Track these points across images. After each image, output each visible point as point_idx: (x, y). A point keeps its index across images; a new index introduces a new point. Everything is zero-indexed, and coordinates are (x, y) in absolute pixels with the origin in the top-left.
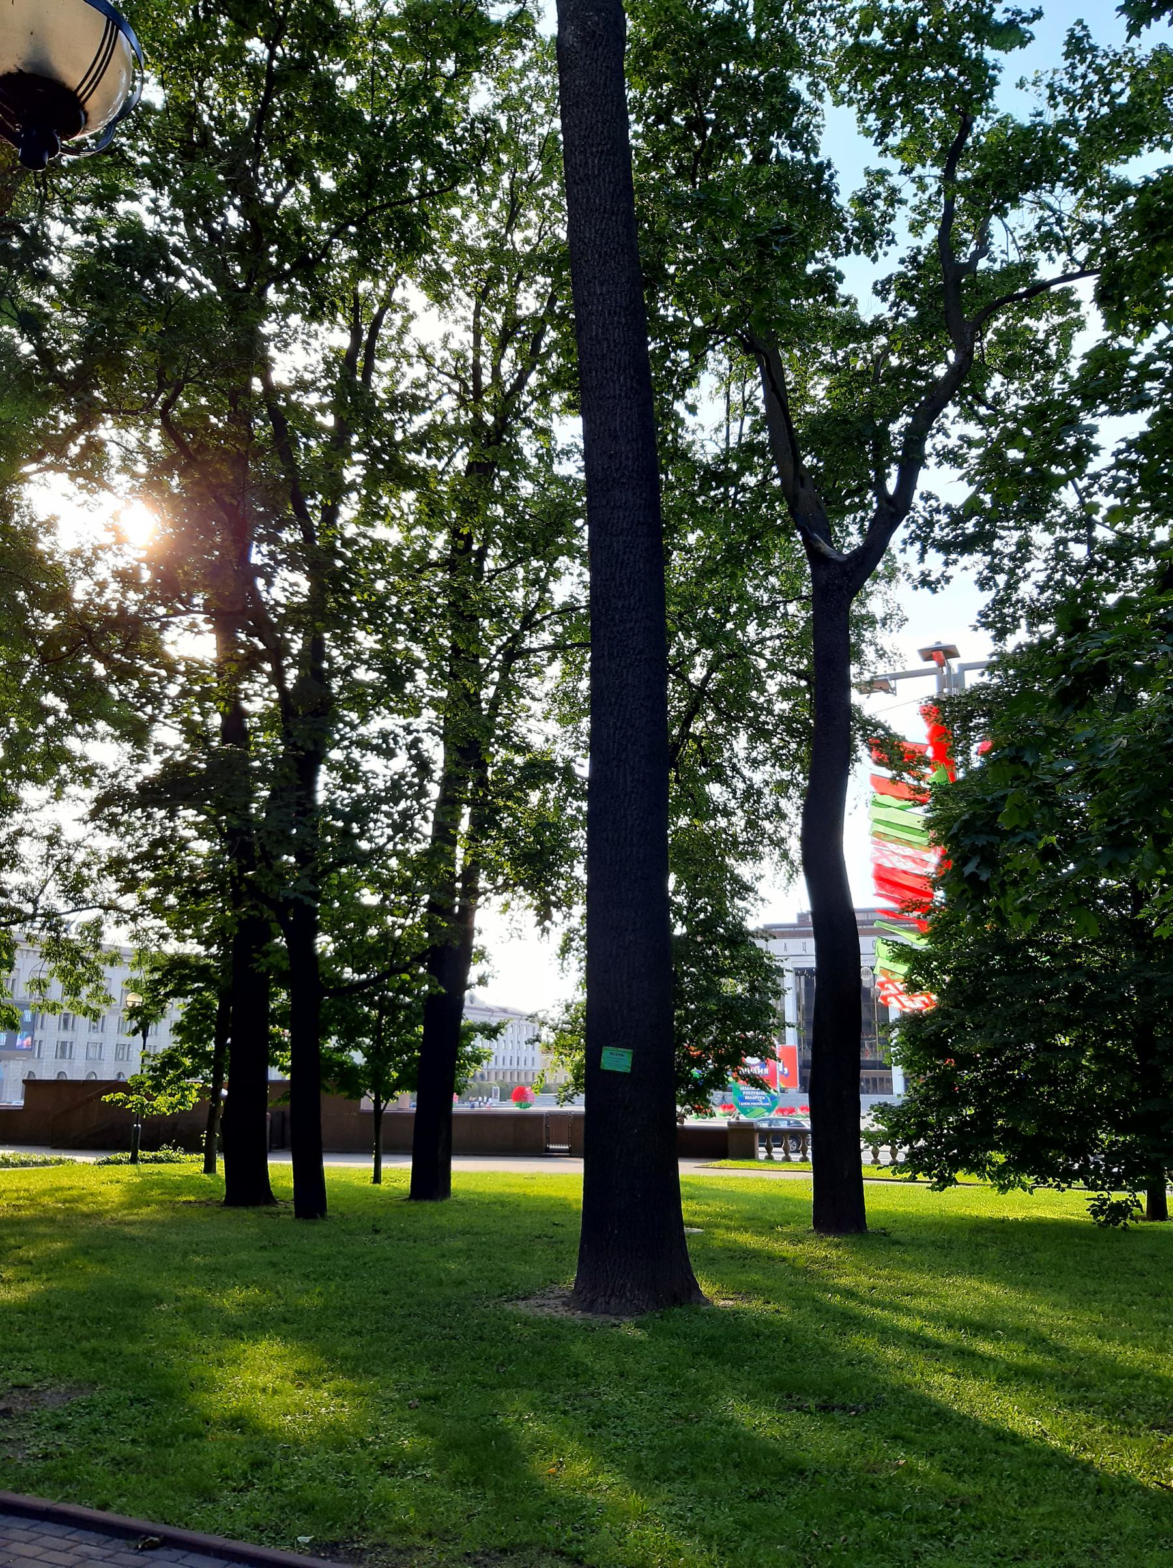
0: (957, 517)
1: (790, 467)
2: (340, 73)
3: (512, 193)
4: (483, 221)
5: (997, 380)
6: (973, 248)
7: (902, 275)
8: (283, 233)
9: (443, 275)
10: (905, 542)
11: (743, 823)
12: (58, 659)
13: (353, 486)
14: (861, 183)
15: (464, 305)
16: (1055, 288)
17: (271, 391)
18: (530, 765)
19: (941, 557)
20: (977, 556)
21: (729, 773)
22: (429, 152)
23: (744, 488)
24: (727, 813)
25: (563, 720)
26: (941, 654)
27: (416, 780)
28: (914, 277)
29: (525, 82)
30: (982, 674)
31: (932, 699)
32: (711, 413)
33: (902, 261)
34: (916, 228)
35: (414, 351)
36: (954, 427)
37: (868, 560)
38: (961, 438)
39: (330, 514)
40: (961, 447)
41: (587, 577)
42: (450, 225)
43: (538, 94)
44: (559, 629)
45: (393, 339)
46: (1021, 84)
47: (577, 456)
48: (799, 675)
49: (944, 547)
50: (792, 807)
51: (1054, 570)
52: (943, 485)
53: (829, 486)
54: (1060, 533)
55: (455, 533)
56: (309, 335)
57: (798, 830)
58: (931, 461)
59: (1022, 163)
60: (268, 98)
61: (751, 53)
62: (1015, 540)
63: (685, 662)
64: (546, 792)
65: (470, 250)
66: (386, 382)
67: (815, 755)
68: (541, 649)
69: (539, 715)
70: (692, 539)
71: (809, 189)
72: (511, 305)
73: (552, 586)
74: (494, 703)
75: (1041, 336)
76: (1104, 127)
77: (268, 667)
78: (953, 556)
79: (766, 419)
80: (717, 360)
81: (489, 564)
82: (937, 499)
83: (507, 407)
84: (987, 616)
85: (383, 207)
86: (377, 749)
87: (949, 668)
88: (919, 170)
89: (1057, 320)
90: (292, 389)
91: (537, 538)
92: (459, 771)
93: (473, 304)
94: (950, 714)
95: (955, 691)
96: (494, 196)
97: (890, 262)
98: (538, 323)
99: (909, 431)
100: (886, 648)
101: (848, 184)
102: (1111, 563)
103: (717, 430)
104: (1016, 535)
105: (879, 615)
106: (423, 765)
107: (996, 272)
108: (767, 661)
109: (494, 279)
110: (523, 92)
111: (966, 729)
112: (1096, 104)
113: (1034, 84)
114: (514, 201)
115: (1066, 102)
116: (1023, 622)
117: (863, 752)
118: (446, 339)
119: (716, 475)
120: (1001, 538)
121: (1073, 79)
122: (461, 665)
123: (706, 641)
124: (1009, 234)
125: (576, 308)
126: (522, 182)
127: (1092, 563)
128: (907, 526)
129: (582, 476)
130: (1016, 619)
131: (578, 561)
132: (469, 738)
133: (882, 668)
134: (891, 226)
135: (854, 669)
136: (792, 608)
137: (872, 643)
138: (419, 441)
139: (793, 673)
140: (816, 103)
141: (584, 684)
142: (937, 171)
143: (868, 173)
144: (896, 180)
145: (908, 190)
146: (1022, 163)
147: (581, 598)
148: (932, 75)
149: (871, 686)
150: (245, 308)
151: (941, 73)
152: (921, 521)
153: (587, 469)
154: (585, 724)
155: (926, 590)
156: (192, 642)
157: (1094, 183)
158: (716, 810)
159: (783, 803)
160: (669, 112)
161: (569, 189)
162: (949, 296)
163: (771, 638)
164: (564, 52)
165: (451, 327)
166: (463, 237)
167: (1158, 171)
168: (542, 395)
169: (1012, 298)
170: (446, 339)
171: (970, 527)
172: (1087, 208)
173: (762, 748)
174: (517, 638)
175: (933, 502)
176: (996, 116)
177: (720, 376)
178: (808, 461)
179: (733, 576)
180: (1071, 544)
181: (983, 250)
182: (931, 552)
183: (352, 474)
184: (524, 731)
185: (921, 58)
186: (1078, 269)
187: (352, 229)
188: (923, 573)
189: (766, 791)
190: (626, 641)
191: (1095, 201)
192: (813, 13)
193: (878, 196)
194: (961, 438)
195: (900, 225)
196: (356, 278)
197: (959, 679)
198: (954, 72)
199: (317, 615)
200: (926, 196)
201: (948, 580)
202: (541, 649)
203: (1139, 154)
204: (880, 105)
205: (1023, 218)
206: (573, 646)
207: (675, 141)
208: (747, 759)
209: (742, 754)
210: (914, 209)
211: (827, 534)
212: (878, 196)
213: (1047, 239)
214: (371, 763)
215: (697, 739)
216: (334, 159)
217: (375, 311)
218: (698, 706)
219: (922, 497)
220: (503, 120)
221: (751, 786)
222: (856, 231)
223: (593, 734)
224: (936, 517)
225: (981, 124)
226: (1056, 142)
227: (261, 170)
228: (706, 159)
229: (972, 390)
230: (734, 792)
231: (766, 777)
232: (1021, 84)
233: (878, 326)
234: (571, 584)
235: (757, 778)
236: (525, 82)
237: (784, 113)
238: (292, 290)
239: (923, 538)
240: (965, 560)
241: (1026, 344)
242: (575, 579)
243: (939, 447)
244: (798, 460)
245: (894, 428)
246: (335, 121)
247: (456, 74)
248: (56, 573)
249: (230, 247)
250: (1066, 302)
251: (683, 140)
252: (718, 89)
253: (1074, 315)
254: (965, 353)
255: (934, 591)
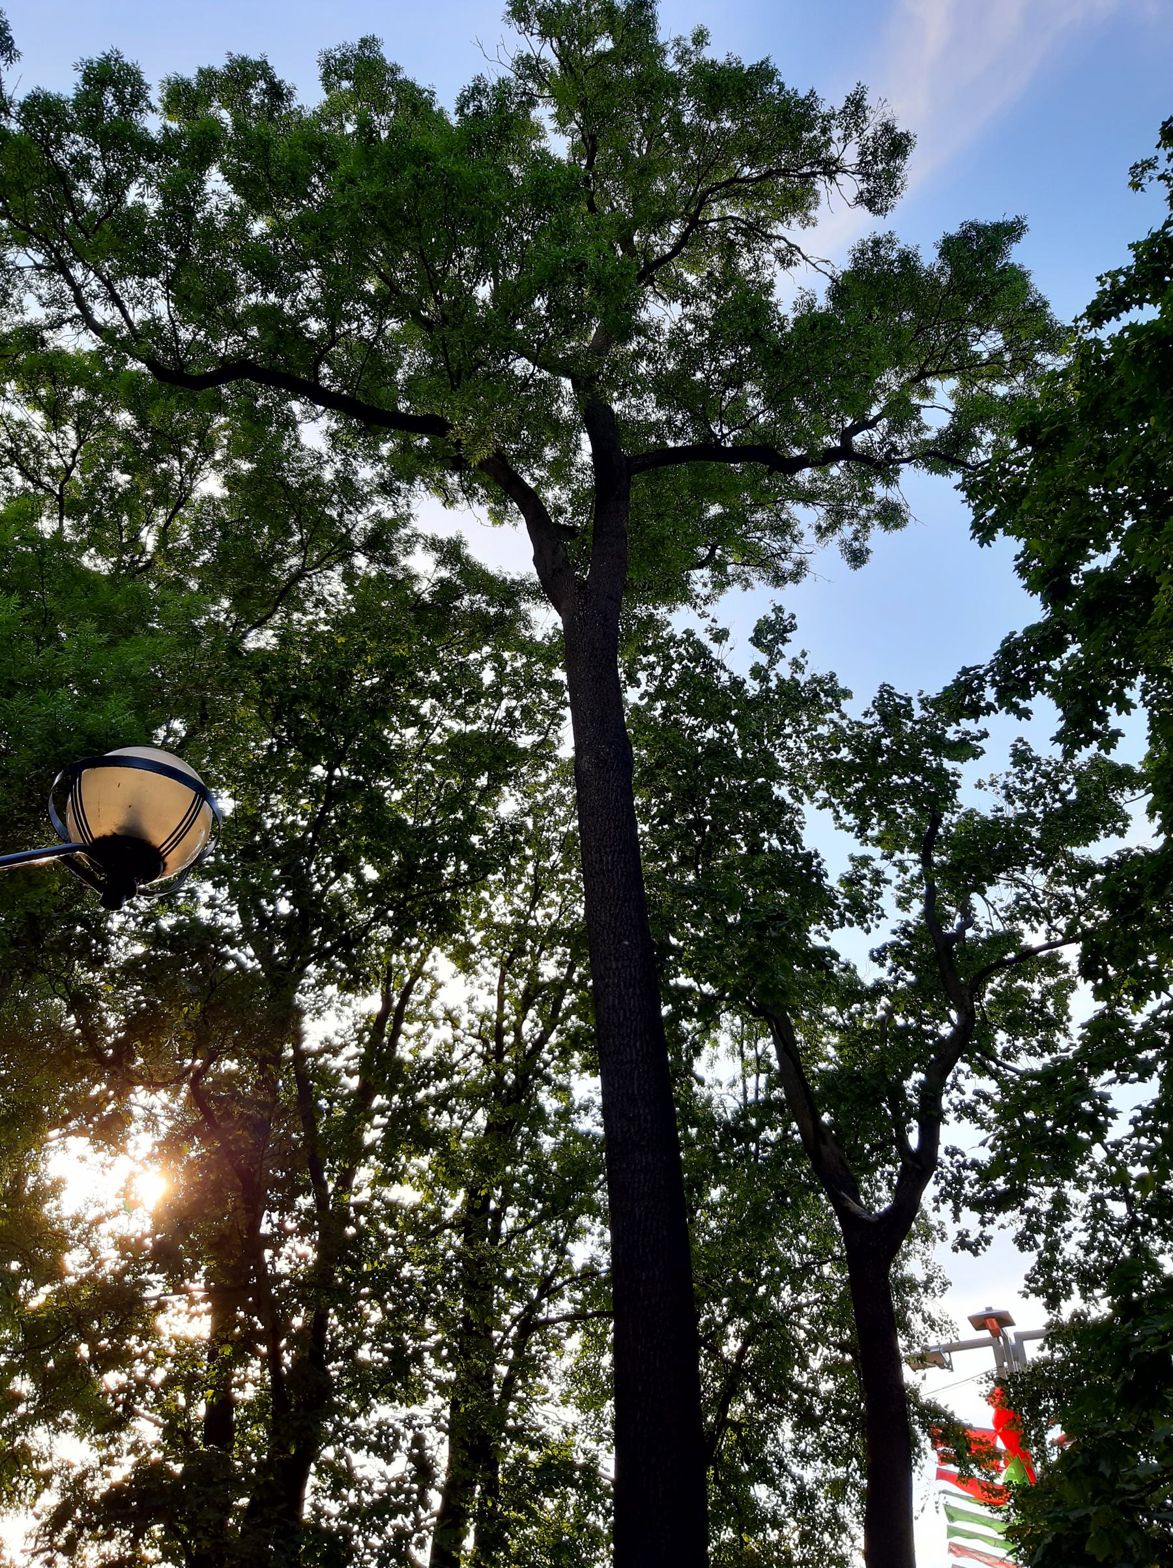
0: (986, 1174)
1: (809, 1124)
2: (388, 788)
3: (535, 877)
5: (1001, 1038)
6: (958, 920)
8: (327, 917)
9: (471, 948)
10: (936, 1200)
11: (796, 1535)
12: (39, 1337)
13: (371, 1149)
14: (848, 867)
15: (489, 972)
16: (1043, 953)
18: (547, 1465)
19: (976, 1216)
22: (463, 851)
23: (766, 1143)
24: (777, 1524)
25: (585, 1404)
27: (415, 1486)
28: (908, 946)
29: (549, 792)
30: (1042, 1349)
31: (989, 1377)
32: (724, 1071)
33: (894, 932)
34: (903, 904)
35: (440, 1014)
36: (968, 1083)
37: (903, 1218)
38: (976, 1093)
39: (345, 1181)
40: (978, 1102)
41: (608, 1237)
44: (579, 1295)
45: (421, 1004)
46: (979, 785)
47: (595, 1110)
48: (843, 1347)
49: (977, 1205)
50: (850, 1512)
51: (1095, 1230)
52: (964, 1140)
53: (850, 1136)
55: (472, 1193)
56: (343, 1004)
57: (861, 1543)
58: (950, 1117)
60: (324, 810)
61: (744, 769)
63: (717, 1335)
64: (565, 1497)
65: (498, 926)
67: (871, 1448)
68: (559, 1320)
69: (557, 1399)
70: (715, 1194)
71: (802, 874)
72: (534, 974)
74: (509, 1382)
75: (1036, 996)
76: (1060, 818)
77: (264, 1349)
79: (780, 1074)
80: (730, 1021)
81: (507, 1224)
82: (963, 1155)
83: (529, 1067)
84: (1036, 1281)
85: (420, 895)
87: (1005, 1338)
88: (898, 856)
89: (1050, 981)
90: (320, 1053)
91: (560, 1201)
92: (466, 1473)
93: (498, 972)
94: (1017, 1393)
95: (1017, 1367)
96: (520, 882)
97: (883, 934)
100: (935, 1316)
102: (1154, 1221)
103: (733, 1084)
104: (1050, 1191)
105: (920, 1277)
106: (423, 1469)
107: (983, 941)
108: (806, 1331)
109: (520, 951)
110: (547, 800)
111: (1036, 1414)
112: (1049, 800)
115: (1022, 800)
116: (1075, 1286)
118: (470, 1001)
119: (739, 1130)
120: (1035, 1195)
121: (1024, 782)
122: (471, 1342)
123: (738, 1310)
124: (990, 907)
126: (545, 869)
127: (1134, 1222)
129: (600, 1131)
130: (1067, 1284)
131: (598, 1220)
132: (479, 1432)
135: (902, 1342)
136: (826, 1270)
137: (917, 1310)
138: (441, 1102)
139: (838, 1346)
141: (607, 1360)
142: (916, 856)
143: (852, 859)
144: (878, 864)
145: (891, 872)
147: (603, 1261)
148: (900, 782)
149: (923, 1360)
150: (282, 980)
151: (908, 780)
154: (609, 1408)
156: (186, 1320)
157: (1062, 863)
158: (765, 1520)
159: (843, 1510)
160: (672, 816)
162: (942, 962)
165: (476, 992)
166: (491, 915)
167: (1118, 853)
168: (565, 1054)
170: (470, 1001)
171: (1000, 1183)
172: (1059, 883)
173: (809, 1442)
174: (533, 1307)
175: (958, 1157)
176: (962, 811)
177: (733, 1036)
178: (826, 1118)
179: (761, 1238)
180: (1108, 1201)
182: (965, 1211)
183: (372, 1136)
184: (540, 1421)
185: (888, 769)
187: (391, 913)
188: (960, 1234)
189: (820, 1493)
190: (651, 1310)
191: (1064, 878)
192: (790, 736)
194: (976, 1093)
195: (888, 899)
198: (918, 778)
200: (908, 877)
201: (988, 1241)
202: (559, 1320)
203: (1096, 839)
205: (1002, 893)
207: (678, 838)
208: (796, 1453)
209: (788, 1447)
210: (898, 888)
211: (855, 1191)
212: (864, 877)
213: (1025, 910)
214: (366, 1465)
215: (737, 1427)
216: (378, 857)
217: (407, 979)
218: (735, 1385)
219: (947, 1152)
220: (529, 822)
221: (801, 1488)
222: (847, 907)
223: (617, 1423)
224: (965, 1173)
225: (948, 818)
226: (1019, 832)
227: (313, 867)
228: (707, 850)
231: (819, 1475)
232: (979, 785)
233: (879, 989)
234: (590, 1247)
235: (810, 1474)
236: (549, 792)
237: (776, 816)
238: (331, 965)
239: (952, 1193)
240: (1002, 1218)
242: (596, 1239)
243: (956, 1102)
244: (817, 1117)
245: (909, 1084)
246: (381, 829)
247: (488, 787)
248: (60, 1242)
249: (278, 931)
250: (1053, 965)
252: (712, 797)
253: (1065, 976)
254: (967, 1014)
255: (976, 1254)
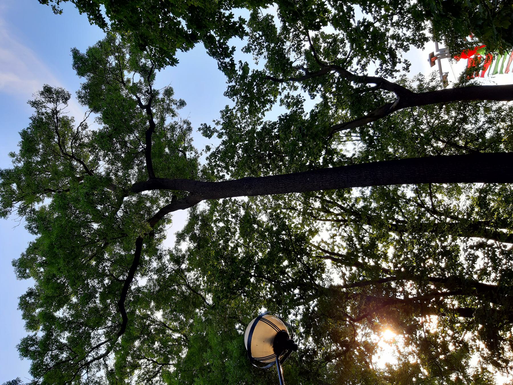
0: (384, 61)
1: (368, 119)
2: (258, 257)
3: (287, 209)
4: (295, 218)
5: (339, 56)
6: (301, 70)
7: (309, 91)
8: (300, 277)
9: (310, 230)
10: (393, 78)
12: (437, 371)
13: (376, 263)
14: (284, 106)
15: (318, 224)
17: (345, 286)
18: (479, 205)
19: (398, 64)
20: (397, 53)
21: (481, 130)
22: (278, 232)
23: (374, 133)
24: (499, 130)
25: (459, 193)
26: (432, 59)
27: (486, 248)
29: (259, 204)
30: (441, 43)
32: (350, 147)
33: (305, 91)
34: (296, 88)
35: (332, 240)
36: (354, 67)
37: (399, 89)
38: (358, 64)
39: (386, 271)
40: (361, 64)
41: (405, 185)
42: (296, 227)
43: (262, 201)
44: (424, 195)
46: (257, 63)
47: (363, 189)
48: (441, 108)
49: (394, 64)
50: (495, 106)
51: (402, 26)
52: (373, 68)
53: (372, 106)
54: (389, 26)
55: (390, 230)
56: (328, 272)
57: (505, 102)
58: (365, 73)
59: (279, 61)
60: (265, 278)
61: (251, 141)
62: (391, 41)
63: (437, 150)
64: (490, 199)
65: (303, 221)
66: (341, 249)
67: (474, 99)
68: (432, 201)
69: (458, 202)
70: (391, 150)
71: (286, 122)
72: (319, 209)
73: (408, 198)
78: (397, 60)
79: (352, 129)
80: (334, 145)
81: (401, 218)
85: (293, 247)
86: (474, 261)
87: (438, 55)
88: (280, 90)
90: (345, 279)
91: (393, 201)
92: (482, 232)
93: (318, 221)
94: (456, 51)
95: (447, 51)
96: (288, 214)
97: (305, 95)
98: (323, 201)
99: (356, 82)
100: (430, 78)
101: (284, 111)
102: (399, 6)
103: (355, 144)
104: (390, 41)
105: (418, 83)
106: (481, 246)
107: (308, 62)
110: (262, 205)
111: (463, 45)
112: (262, 41)
113: (257, 60)
114: (289, 208)
115: (262, 49)
116: (421, 32)
117: (472, 81)
118: (327, 230)
119: (370, 142)
121: (256, 49)
122: (439, 230)
124: (297, 60)
125: (319, 190)
127: (400, 13)
128: (387, 77)
129: (370, 188)
130: (420, 35)
131: (399, 188)
132: (469, 228)
133: (438, 78)
134: (295, 96)
135: (439, 89)
137: (429, 84)
138: (361, 240)
140: (263, 123)
141: (445, 186)
142: (280, 84)
143: (281, 105)
144: (283, 96)
145: (285, 93)
146: (279, 61)
149: (445, 81)
150: (320, 292)
151: (255, 87)
152: (385, 73)
153: (368, 185)
154: (461, 185)
155: (410, 68)
156: (432, 323)
158: (497, 134)
159: (494, 108)
160: (267, 164)
161: (286, 192)
162: (315, 75)
163: (427, 120)
164: (252, 195)
165: (324, 228)
167: (279, 18)
168: (345, 199)
169: (315, 56)
171: (387, 57)
172: (289, 37)
173: (472, 119)
174: (427, 209)
176: (265, 69)
177: (339, 144)
180: (393, 21)
181: (301, 67)
183: (372, 263)
184: (465, 207)
185: (252, 93)
186: (307, 37)
187: (299, 256)
188: (404, 70)
189: (489, 115)
190: (430, 171)
193: (287, 101)
194: (358, 64)
195: (294, 93)
196: (311, 257)
197: (443, 51)
199: (421, 280)
201: (406, 61)
202: (432, 201)
204: (264, 104)
205: (292, 56)
206: (430, 190)
207: (274, 162)
208: (475, 124)
209: (473, 126)
210: (291, 90)
211: (390, 104)
212: (287, 101)
213: (298, 48)
214: (479, 264)
216: (280, 260)
217: (320, 251)
220: (269, 211)
221: (487, 122)
222: (297, 107)
223: (466, 182)
224: (384, 68)
225: (268, 74)
226: (272, 51)
227: (284, 282)
228: (278, 153)
229: (343, 64)
230: (489, 128)
232: (257, 63)
233: (324, 96)
234: (408, 191)
235: (482, 119)
236: (259, 204)
238: (316, 276)
239: (391, 72)
240: (399, 56)
241: (329, 48)
242: (405, 189)
243: (360, 71)
246: (271, 259)
247: (257, 224)
249: (305, 293)
250: (316, 39)
251: (274, 160)
253: (319, 35)
254: (332, 67)
255: (410, 65)
